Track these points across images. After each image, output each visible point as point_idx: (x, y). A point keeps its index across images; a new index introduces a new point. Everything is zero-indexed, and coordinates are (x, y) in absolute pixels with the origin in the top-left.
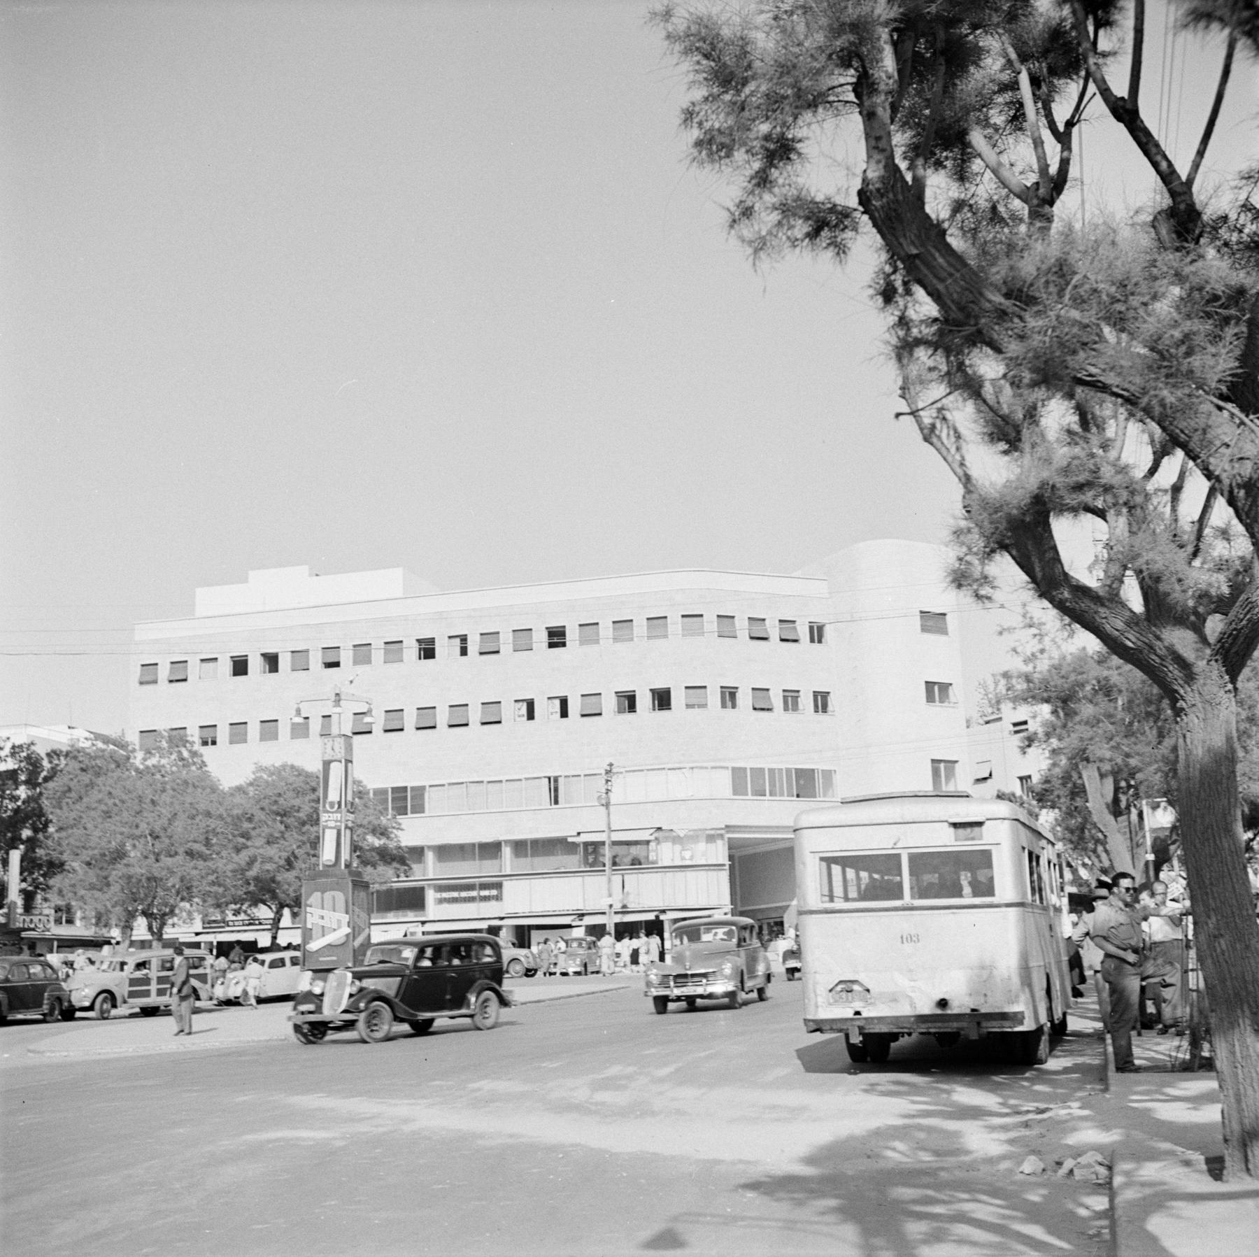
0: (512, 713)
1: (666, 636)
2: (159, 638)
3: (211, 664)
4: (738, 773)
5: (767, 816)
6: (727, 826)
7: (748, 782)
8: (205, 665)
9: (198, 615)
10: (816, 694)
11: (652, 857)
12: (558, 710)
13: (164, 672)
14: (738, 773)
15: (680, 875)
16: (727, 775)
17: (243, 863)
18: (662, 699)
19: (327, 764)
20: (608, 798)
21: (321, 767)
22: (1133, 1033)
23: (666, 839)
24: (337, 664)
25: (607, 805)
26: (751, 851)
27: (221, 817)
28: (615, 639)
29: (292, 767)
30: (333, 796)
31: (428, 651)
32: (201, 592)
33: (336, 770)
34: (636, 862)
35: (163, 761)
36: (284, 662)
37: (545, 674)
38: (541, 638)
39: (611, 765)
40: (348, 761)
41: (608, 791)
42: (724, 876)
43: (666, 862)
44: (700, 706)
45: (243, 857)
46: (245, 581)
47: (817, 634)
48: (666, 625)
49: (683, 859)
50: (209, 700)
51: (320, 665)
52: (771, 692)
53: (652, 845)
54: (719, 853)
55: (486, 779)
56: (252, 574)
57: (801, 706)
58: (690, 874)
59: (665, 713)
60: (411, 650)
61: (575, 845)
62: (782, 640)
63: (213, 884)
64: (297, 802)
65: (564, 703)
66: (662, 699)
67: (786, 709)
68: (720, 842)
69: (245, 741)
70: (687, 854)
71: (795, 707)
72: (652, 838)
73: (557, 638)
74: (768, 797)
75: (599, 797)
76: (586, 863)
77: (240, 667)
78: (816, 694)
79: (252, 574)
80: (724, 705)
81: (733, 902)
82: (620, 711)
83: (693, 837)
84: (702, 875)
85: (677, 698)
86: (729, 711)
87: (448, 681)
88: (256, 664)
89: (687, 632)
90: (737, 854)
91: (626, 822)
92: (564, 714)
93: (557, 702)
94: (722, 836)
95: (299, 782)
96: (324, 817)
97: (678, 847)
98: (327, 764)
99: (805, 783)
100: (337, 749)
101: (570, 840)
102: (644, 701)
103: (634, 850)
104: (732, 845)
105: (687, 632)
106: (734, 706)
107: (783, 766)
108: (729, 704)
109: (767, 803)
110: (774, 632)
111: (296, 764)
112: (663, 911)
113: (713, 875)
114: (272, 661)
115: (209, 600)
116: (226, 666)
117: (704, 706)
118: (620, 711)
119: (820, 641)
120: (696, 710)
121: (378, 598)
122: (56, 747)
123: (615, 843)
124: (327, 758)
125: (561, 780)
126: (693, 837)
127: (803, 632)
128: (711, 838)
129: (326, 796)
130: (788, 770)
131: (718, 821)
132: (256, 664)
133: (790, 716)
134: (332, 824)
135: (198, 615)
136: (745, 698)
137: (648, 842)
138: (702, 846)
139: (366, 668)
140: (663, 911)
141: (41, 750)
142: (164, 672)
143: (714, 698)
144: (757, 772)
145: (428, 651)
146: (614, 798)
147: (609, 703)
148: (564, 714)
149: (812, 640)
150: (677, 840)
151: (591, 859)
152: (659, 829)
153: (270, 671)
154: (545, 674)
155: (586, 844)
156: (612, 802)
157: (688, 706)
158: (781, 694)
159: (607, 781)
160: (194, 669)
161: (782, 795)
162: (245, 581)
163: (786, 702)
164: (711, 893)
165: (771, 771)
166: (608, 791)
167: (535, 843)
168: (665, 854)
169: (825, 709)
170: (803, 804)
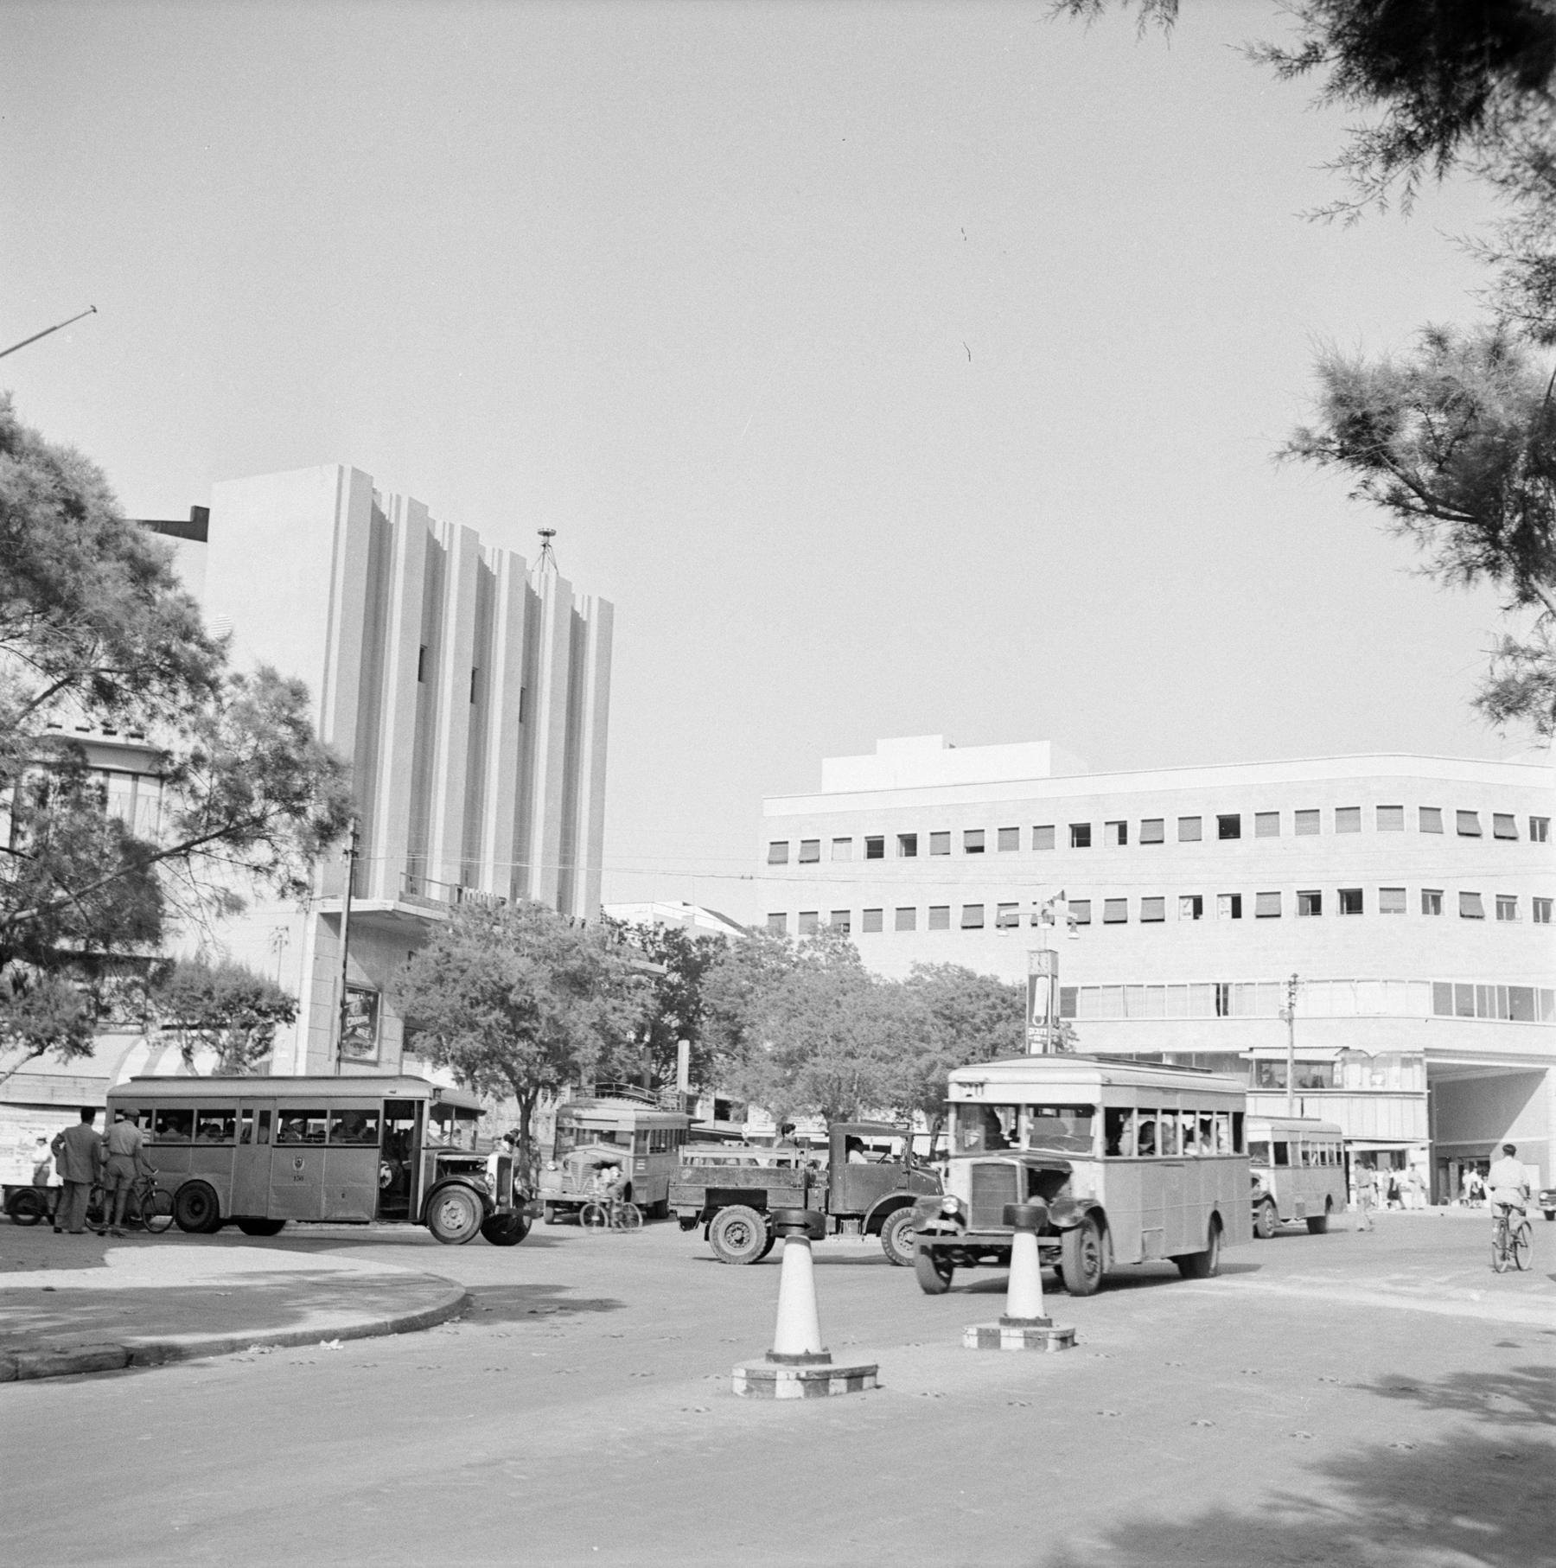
0: (1178, 911)
1: (1358, 830)
2: (789, 816)
3: (845, 845)
4: (1441, 990)
5: (1483, 1041)
6: (1426, 1050)
7: (1455, 1000)
8: (838, 845)
9: (824, 791)
10: (1536, 901)
11: (1337, 1079)
12: (1229, 908)
13: (794, 851)
14: (1441, 990)
15: (1369, 1102)
16: (1428, 992)
17: (923, 1067)
18: (1352, 901)
19: (1033, 979)
20: (1291, 1013)
21: (1026, 981)
22: (55, 1180)
23: (1354, 1061)
24: (981, 849)
25: (1290, 1021)
26: (1451, 1078)
27: (901, 1020)
28: (1298, 833)
29: (962, 970)
30: (1040, 1010)
31: (1082, 835)
32: (828, 764)
33: (1043, 986)
34: (1317, 1083)
35: (818, 954)
36: (923, 845)
37: (1217, 868)
38: (1211, 828)
39: (1295, 976)
40: (1055, 976)
41: (1291, 1005)
42: (1422, 1107)
43: (1353, 1086)
44: (1398, 911)
45: (923, 1062)
46: (872, 750)
47: (1539, 829)
48: (1359, 818)
49: (1373, 1084)
50: (846, 884)
51: (962, 850)
52: (1482, 897)
53: (1337, 1067)
54: (1417, 1080)
55: (1146, 983)
56: (881, 744)
57: (1517, 914)
58: (1381, 1102)
59: (1355, 917)
60: (1064, 836)
61: (1248, 1062)
62: (1497, 837)
63: (897, 1087)
64: (971, 1008)
65: (1236, 901)
66: (1352, 901)
67: (1500, 916)
68: (1417, 1067)
69: (880, 930)
70: (1378, 1079)
71: (1511, 915)
72: (1338, 1058)
73: (1229, 828)
74: (1476, 1018)
75: (1282, 1012)
76: (1260, 1082)
77: (875, 849)
78: (1536, 901)
79: (881, 744)
80: (1425, 911)
81: (1431, 1137)
82: (1303, 912)
83: (1387, 1060)
84: (1395, 1103)
85: (1370, 901)
86: (1431, 917)
87: (1106, 871)
88: (892, 846)
89: (1382, 825)
90: (1439, 1079)
91: (1312, 1042)
92: (1237, 913)
93: (1229, 900)
94: (1420, 1060)
95: (972, 987)
96: (1030, 1031)
97: (1367, 1071)
98: (1033, 979)
99: (1519, 1003)
100: (1043, 963)
101: (1242, 1056)
102: (1331, 902)
103: (1315, 1071)
104: (1432, 1071)
105: (1382, 825)
106: (1437, 912)
107: (1495, 983)
108: (1432, 909)
109: (1475, 1025)
110: (1487, 825)
111: (967, 967)
112: (1349, 1142)
113: (1408, 1104)
114: (909, 844)
115: (839, 773)
116: (861, 848)
117: (1401, 911)
118: (1303, 912)
119: (1543, 839)
120: (1392, 915)
121: (1020, 775)
122: (705, 934)
123: (1298, 1062)
124: (1034, 972)
125: (1231, 990)
126: (1387, 1060)
127: (1522, 827)
128: (1407, 1062)
129: (1032, 1011)
130: (1501, 989)
131: (1416, 1042)
132: (892, 846)
133: (1504, 925)
134: (1038, 1038)
135: (824, 791)
136: (1450, 903)
137: (1333, 1063)
138: (1396, 1070)
139: (1013, 854)
140: (1349, 1142)
141: (692, 936)
142: (794, 851)
143: (1414, 902)
144: (1465, 990)
145: (1082, 835)
146: (1297, 1012)
147: (1290, 903)
148: (1237, 913)
149: (1533, 838)
150: (1369, 1060)
151: (1265, 1078)
152: (1346, 1048)
153: (907, 855)
154: (1217, 868)
155: (1260, 1062)
156: (1296, 1015)
157: (1383, 910)
158: (1495, 899)
159: (1291, 994)
160: (826, 849)
161: (1493, 1016)
162: (872, 750)
163: (1499, 911)
164: (1408, 1123)
165: (1481, 988)
166: (1291, 1005)
167: (1201, 1057)
168: (1353, 1076)
169: (1546, 918)
170: (1518, 1026)
